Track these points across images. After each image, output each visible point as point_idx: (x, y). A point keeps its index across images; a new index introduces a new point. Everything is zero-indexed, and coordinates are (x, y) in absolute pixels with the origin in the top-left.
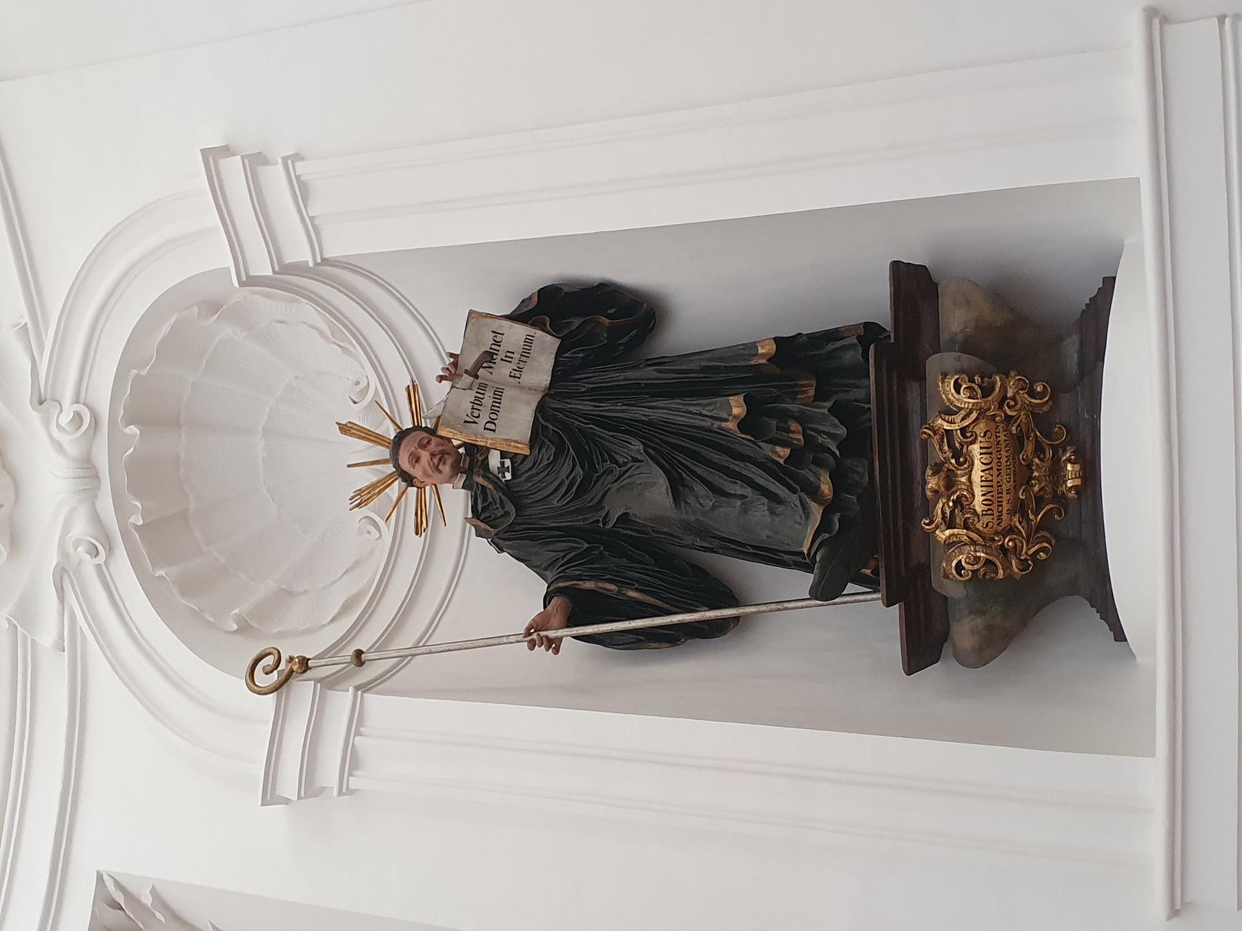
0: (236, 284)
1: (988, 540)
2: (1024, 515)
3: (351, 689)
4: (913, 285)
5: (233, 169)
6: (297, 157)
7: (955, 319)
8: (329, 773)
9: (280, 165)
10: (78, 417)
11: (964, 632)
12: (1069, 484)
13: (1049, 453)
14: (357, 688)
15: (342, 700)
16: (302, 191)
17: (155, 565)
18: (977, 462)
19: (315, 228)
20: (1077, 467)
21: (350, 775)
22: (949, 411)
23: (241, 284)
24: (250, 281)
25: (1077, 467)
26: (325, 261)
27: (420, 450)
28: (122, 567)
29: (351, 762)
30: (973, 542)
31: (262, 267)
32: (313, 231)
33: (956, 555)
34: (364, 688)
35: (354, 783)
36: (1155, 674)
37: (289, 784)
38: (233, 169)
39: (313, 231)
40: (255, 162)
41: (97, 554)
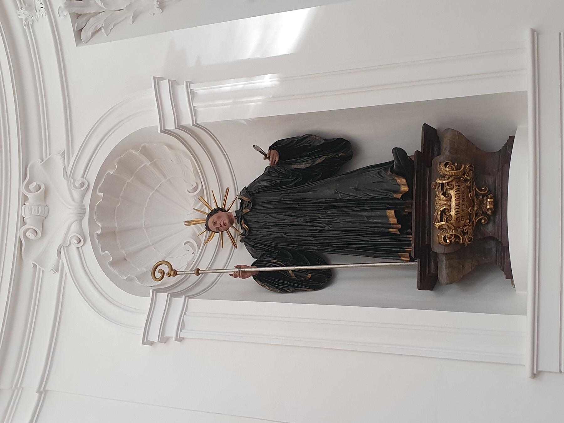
0: (159, 132)
1: (456, 228)
2: (470, 219)
3: (183, 296)
4: (430, 135)
5: (165, 85)
6: (191, 83)
7: (446, 144)
8: (171, 332)
9: (185, 85)
10: (83, 184)
11: (444, 273)
12: (488, 207)
13: (481, 197)
14: (186, 297)
15: (179, 302)
16: (192, 95)
17: (103, 250)
18: (453, 197)
19: (195, 111)
20: (492, 200)
21: (181, 331)
22: (443, 177)
23: (162, 131)
24: (165, 131)
25: (492, 200)
26: (197, 125)
27: (215, 220)
28: (88, 249)
29: (181, 325)
30: (450, 228)
31: (171, 125)
32: (194, 112)
33: (441, 236)
34: (190, 297)
35: (183, 335)
36: (527, 96)
37: (154, 336)
38: (165, 85)
39: (194, 112)
40: (173, 84)
41: (80, 241)
